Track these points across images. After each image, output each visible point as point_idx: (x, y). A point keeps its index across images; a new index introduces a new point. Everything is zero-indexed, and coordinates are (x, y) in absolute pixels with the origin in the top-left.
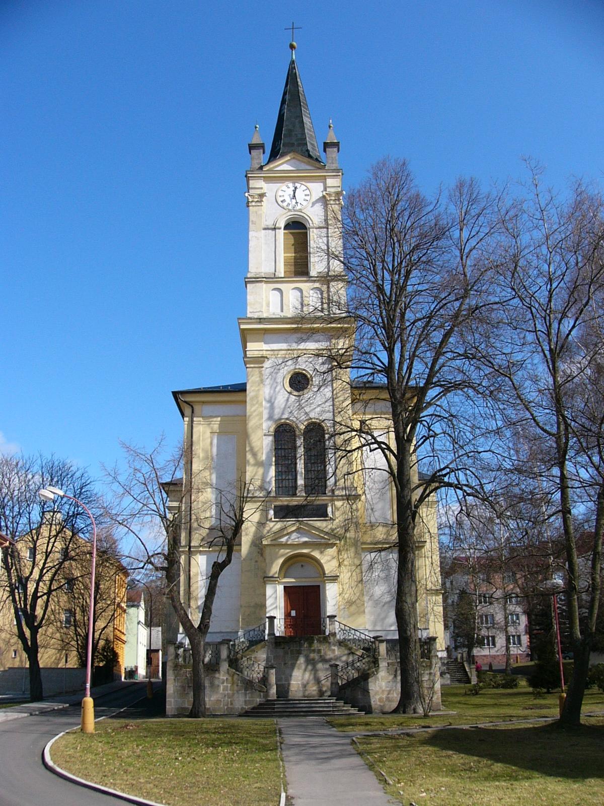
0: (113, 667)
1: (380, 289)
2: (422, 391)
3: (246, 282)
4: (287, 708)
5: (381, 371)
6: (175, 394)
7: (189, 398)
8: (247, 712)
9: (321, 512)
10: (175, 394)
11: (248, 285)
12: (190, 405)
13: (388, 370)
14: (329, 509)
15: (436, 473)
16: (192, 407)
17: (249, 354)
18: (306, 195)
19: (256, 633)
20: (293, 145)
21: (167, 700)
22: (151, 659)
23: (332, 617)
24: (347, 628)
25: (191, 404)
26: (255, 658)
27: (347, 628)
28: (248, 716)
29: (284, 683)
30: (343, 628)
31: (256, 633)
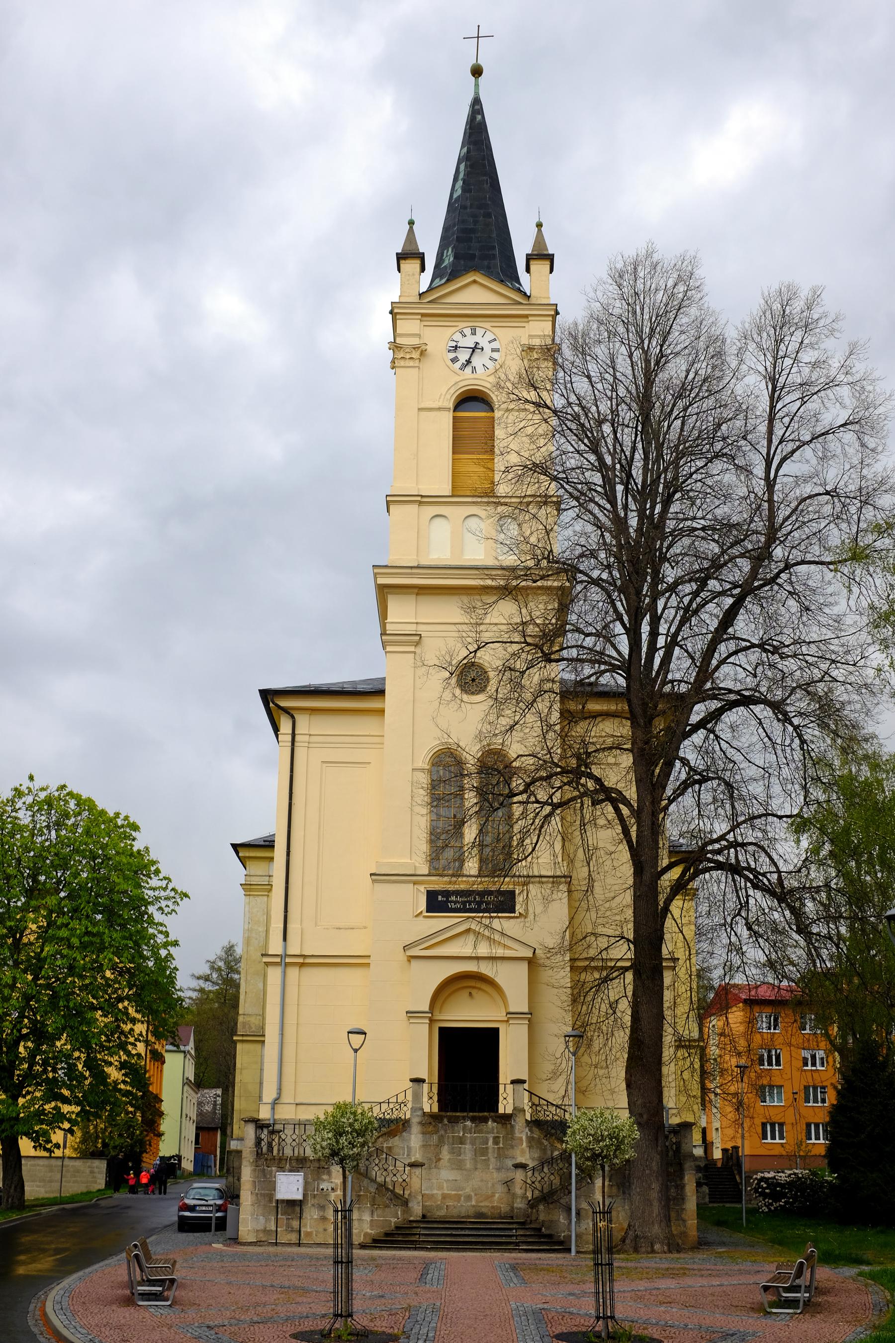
0: (142, 1152)
1: (620, 524)
2: (683, 703)
3: (387, 502)
4: (462, 1229)
5: (619, 668)
6: (267, 695)
7: (284, 703)
8: (375, 1241)
9: (505, 903)
10: (267, 695)
11: (392, 507)
12: (288, 713)
13: (629, 666)
14: (519, 899)
15: (706, 844)
16: (293, 717)
17: (390, 628)
18: (493, 350)
19: (391, 1106)
20: (473, 257)
21: (241, 1217)
22: (256, 1146)
23: (814, 1174)
24: (542, 1102)
25: (292, 712)
26: (390, 1148)
27: (542, 1102)
28: (392, 1242)
29: (435, 1192)
30: (537, 1102)
31: (391, 1106)
